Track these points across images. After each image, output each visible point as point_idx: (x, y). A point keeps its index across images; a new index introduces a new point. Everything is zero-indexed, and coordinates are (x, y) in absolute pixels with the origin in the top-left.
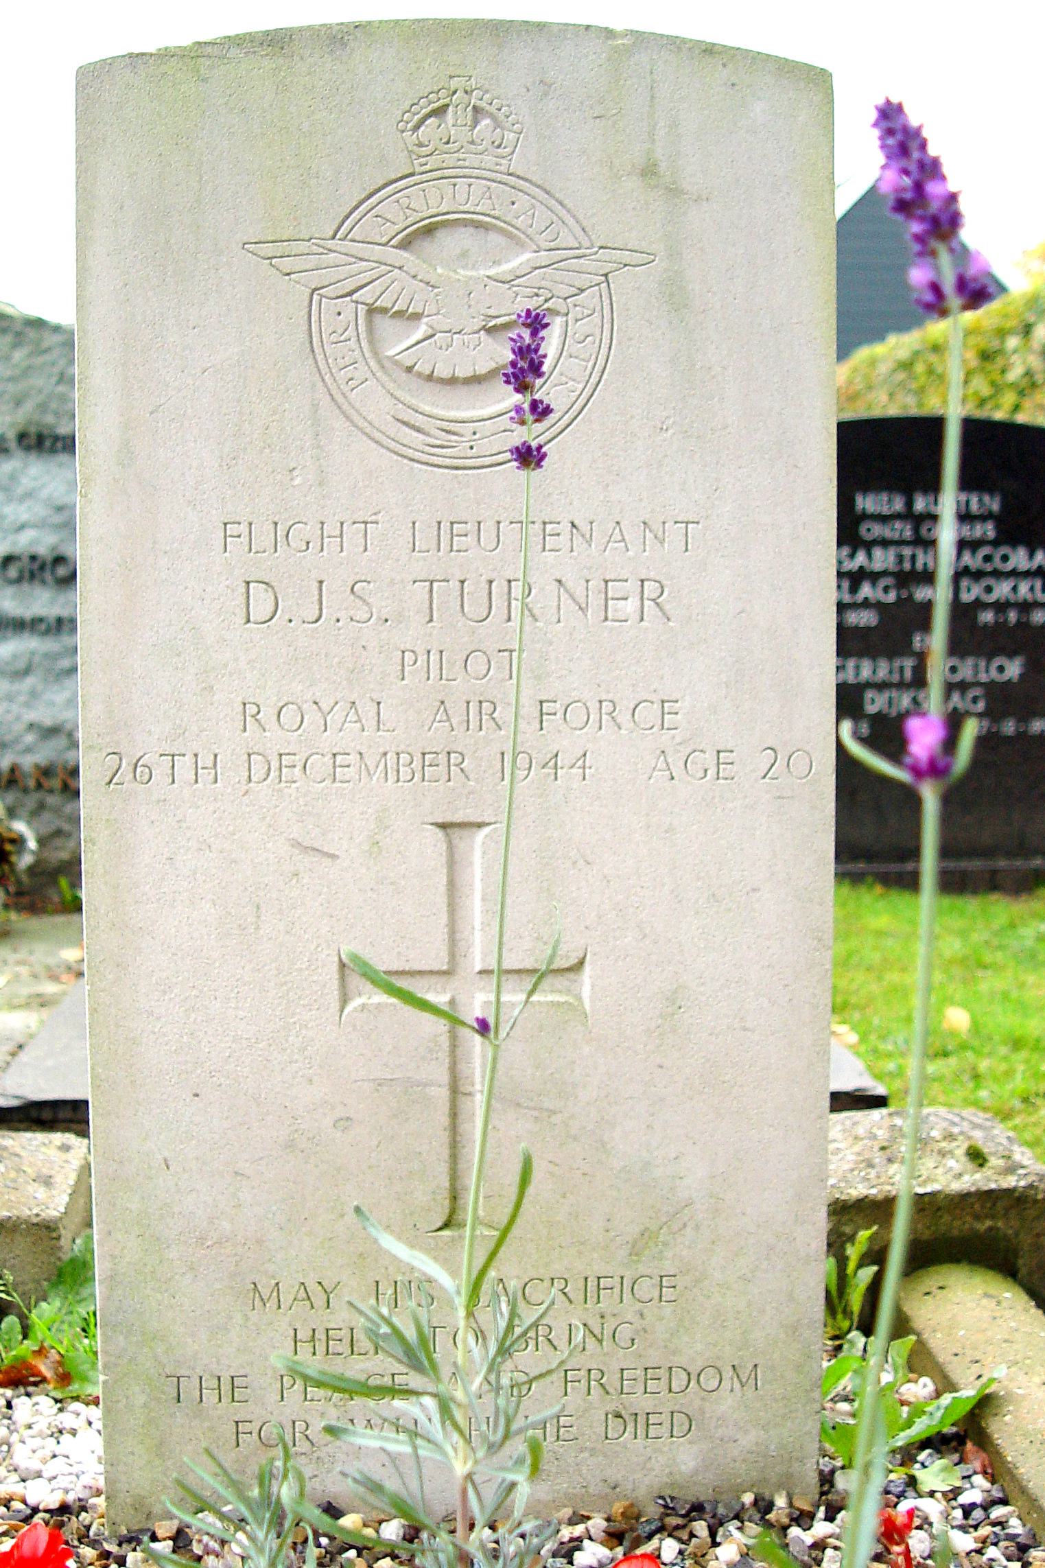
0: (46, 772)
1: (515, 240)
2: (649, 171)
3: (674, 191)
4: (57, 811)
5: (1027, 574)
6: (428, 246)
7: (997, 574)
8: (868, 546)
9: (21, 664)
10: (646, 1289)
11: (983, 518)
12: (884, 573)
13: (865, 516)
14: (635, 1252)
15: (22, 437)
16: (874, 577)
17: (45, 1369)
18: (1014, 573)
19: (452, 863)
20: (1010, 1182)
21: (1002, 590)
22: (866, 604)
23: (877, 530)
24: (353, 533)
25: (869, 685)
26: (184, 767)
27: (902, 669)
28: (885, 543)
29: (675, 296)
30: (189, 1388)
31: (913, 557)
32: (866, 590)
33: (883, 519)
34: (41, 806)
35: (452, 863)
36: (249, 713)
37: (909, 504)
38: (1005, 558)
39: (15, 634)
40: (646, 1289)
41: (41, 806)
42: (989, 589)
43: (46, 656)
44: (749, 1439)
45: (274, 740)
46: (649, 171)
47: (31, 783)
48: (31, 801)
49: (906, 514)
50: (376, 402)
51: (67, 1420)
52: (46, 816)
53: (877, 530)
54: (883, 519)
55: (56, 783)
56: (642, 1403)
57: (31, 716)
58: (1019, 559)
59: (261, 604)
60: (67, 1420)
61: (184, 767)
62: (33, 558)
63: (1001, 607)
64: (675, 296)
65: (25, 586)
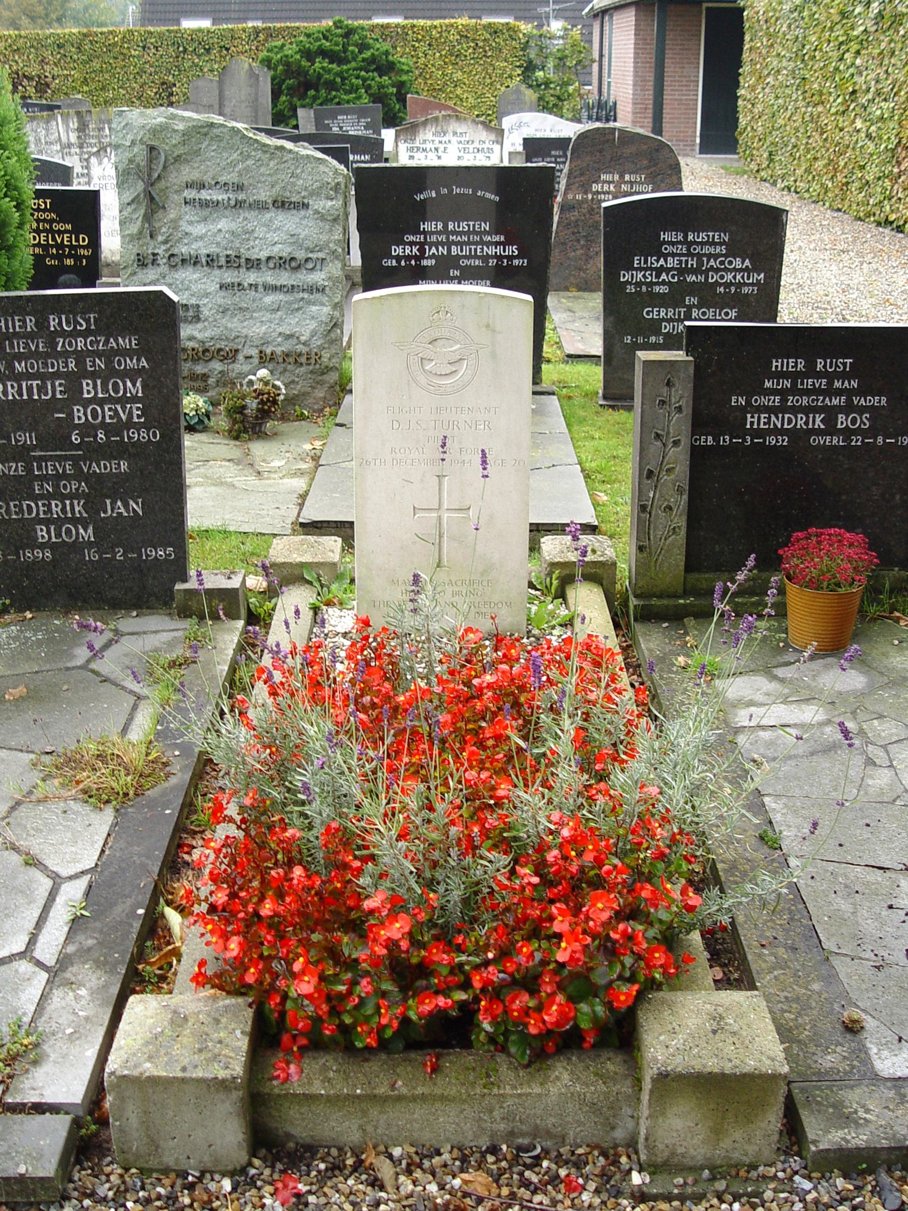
0: (287, 355)
1: (456, 342)
2: (488, 326)
3: (494, 331)
4: (291, 372)
5: (741, 270)
6: (436, 343)
7: (726, 270)
8: (665, 257)
9: (276, 306)
10: (485, 583)
11: (720, 244)
12: (673, 269)
13: (664, 242)
14: (482, 574)
15: (275, 202)
16: (668, 270)
17: (335, 601)
18: (735, 270)
19: (440, 484)
20: (601, 559)
21: (729, 277)
22: (664, 283)
23: (670, 249)
24: (417, 410)
25: (663, 320)
26: (378, 462)
27: (680, 312)
28: (673, 255)
29: (494, 356)
30: (377, 604)
31: (687, 261)
32: (663, 276)
33: (673, 244)
34: (285, 370)
35: (440, 484)
36: (393, 450)
37: (686, 237)
38: (730, 263)
39: (639, 1050)
40: (485, 583)
41: (285, 370)
42: (722, 277)
43: (286, 302)
44: (509, 619)
45: (399, 456)
46: (488, 326)
47: (281, 360)
48: (280, 368)
49: (685, 242)
50: (422, 379)
51: (342, 614)
52: (287, 374)
53: (670, 249)
54: (673, 244)
55: (291, 360)
56: (484, 610)
57: (280, 330)
58: (737, 263)
59: (396, 425)
60: (342, 614)
61: (378, 462)
62: (281, 258)
63: (727, 285)
64: (494, 356)
65: (277, 271)
